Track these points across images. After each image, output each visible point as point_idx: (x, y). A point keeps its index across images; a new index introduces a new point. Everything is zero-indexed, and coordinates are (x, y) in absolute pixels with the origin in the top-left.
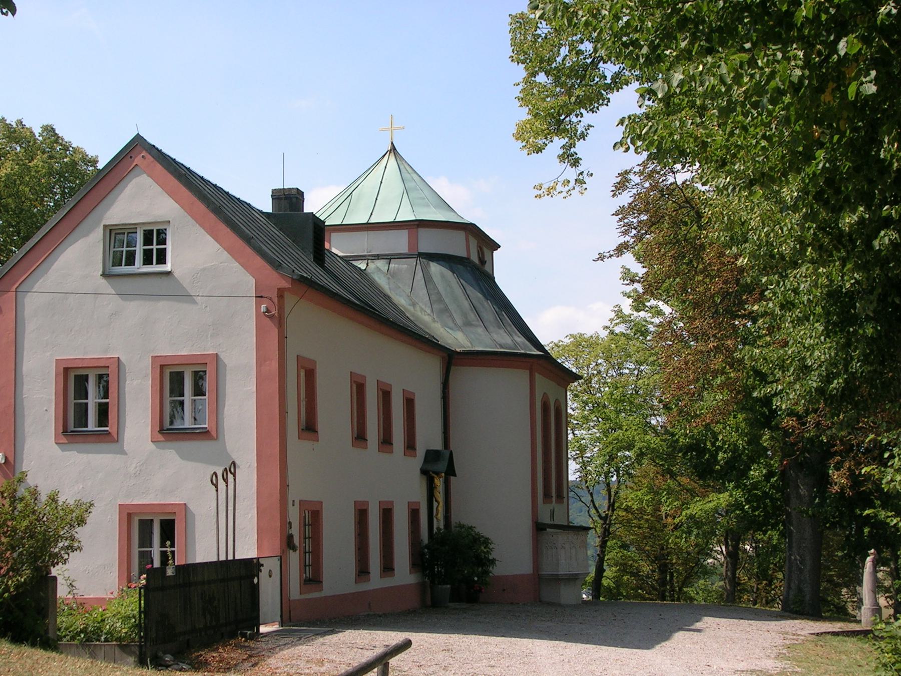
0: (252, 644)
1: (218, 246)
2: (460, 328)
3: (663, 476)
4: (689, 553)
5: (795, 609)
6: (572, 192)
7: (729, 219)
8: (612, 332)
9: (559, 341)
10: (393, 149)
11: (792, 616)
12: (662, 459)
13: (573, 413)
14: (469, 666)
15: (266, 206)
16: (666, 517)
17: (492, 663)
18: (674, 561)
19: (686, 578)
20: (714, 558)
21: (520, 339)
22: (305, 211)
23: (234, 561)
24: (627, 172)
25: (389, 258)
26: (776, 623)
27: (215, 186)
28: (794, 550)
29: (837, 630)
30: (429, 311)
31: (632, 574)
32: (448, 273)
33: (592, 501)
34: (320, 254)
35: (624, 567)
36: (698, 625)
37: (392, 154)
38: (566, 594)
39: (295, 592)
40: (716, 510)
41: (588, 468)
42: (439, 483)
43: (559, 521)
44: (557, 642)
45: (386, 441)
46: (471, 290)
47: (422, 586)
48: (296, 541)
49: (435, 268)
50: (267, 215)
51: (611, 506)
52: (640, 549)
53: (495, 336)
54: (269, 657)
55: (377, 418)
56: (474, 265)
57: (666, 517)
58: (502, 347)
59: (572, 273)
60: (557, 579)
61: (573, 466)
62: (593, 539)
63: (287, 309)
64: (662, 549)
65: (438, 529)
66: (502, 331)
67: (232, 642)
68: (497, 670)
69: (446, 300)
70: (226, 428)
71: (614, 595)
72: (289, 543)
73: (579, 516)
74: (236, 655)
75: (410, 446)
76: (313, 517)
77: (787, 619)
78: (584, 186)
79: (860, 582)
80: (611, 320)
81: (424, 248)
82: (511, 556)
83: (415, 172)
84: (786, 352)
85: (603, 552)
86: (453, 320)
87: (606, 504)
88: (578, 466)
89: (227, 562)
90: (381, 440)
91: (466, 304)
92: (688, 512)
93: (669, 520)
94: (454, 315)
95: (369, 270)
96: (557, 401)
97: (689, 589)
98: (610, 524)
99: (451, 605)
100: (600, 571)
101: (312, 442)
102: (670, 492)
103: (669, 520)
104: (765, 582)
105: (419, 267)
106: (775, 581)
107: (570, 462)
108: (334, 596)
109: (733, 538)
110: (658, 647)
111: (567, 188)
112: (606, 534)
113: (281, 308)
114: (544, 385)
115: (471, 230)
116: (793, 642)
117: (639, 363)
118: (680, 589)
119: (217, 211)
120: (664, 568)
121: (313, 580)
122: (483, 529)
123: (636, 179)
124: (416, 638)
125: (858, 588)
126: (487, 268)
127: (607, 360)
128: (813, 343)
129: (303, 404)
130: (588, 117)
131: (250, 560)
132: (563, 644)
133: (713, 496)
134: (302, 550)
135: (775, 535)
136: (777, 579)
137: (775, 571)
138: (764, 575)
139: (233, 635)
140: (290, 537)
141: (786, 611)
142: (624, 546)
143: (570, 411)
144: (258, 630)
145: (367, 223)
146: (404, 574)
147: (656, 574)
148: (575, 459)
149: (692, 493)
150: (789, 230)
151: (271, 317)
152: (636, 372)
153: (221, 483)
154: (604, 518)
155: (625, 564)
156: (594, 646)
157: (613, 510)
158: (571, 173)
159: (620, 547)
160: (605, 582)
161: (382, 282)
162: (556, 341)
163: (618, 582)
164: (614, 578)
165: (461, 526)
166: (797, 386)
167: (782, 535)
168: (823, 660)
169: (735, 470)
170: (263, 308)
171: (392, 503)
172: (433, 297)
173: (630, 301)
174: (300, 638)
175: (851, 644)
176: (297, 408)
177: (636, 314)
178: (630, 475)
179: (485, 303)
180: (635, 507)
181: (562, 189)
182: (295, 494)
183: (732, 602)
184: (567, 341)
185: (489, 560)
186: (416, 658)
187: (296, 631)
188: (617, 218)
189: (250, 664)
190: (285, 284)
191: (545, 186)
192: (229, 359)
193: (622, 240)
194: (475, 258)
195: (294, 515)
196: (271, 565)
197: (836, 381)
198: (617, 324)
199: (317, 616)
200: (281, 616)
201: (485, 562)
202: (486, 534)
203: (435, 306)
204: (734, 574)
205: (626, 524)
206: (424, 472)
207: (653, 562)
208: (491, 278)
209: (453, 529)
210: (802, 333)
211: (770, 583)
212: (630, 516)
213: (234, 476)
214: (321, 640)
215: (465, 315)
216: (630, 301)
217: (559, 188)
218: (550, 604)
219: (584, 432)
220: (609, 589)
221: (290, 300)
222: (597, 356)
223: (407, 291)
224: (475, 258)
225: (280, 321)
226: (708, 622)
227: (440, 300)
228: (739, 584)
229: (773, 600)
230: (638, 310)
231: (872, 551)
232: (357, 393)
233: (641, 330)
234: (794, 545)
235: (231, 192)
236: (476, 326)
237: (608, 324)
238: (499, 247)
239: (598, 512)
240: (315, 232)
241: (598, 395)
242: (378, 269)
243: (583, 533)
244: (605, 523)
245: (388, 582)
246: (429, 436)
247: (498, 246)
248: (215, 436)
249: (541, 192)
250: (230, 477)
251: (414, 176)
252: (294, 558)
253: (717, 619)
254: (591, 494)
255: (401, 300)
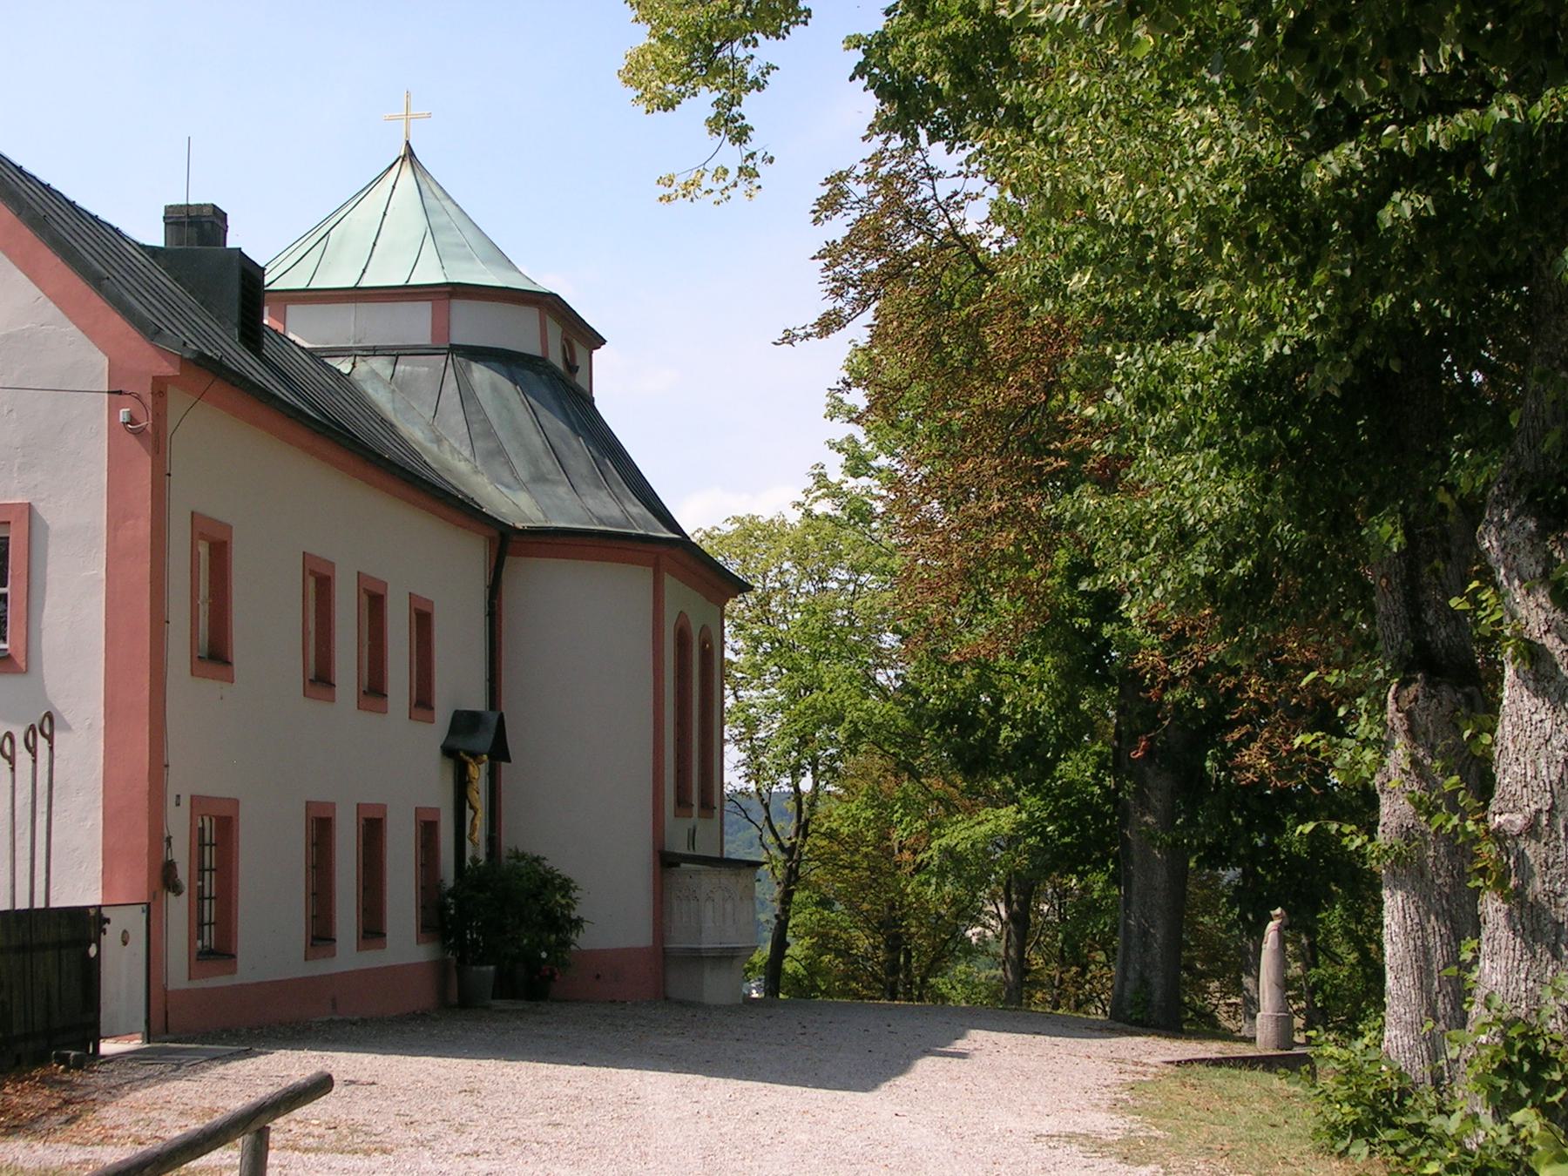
0: (76, 1077)
1: (37, 291)
2: (524, 486)
3: (896, 776)
4: (940, 917)
5: (1134, 1016)
6: (732, 192)
7: (1055, 187)
8: (808, 513)
9: (714, 529)
10: (410, 155)
11: (1129, 1028)
12: (895, 744)
13: (735, 659)
14: (510, 1124)
15: (153, 234)
16: (900, 851)
17: (557, 1118)
18: (913, 930)
19: (935, 960)
20: (984, 925)
21: (637, 509)
22: (229, 245)
23: (48, 911)
24: (841, 177)
25: (396, 353)
26: (1102, 1041)
27: (47, 187)
28: (1134, 908)
29: (1215, 1056)
30: (467, 453)
31: (838, 953)
32: (506, 385)
33: (768, 818)
34: (252, 335)
35: (824, 941)
36: (960, 1045)
37: (407, 162)
38: (715, 986)
39: (178, 973)
40: (991, 838)
41: (762, 759)
42: (478, 773)
43: (701, 850)
44: (689, 1076)
45: (374, 690)
46: (547, 417)
47: (441, 968)
48: (183, 873)
49: (481, 374)
50: (153, 251)
51: (803, 829)
52: (852, 906)
53: (590, 503)
54: (105, 1104)
55: (355, 646)
56: (550, 369)
57: (900, 851)
58: (601, 522)
59: (741, 408)
60: (696, 958)
61: (733, 755)
62: (768, 889)
63: (171, 423)
64: (892, 908)
65: (475, 860)
66: (603, 494)
67: (38, 1073)
68: (564, 1133)
69: (500, 434)
70: (44, 648)
71: (804, 989)
72: (167, 878)
73: (738, 845)
74: (38, 1099)
75: (423, 702)
76: (219, 831)
77: (1120, 1035)
78: (757, 181)
79: (1253, 967)
80: (807, 492)
81: (462, 335)
82: (613, 910)
83: (449, 198)
84: (1146, 505)
85: (785, 911)
86: (513, 471)
87: (791, 828)
88: (743, 756)
89: (31, 913)
90: (365, 687)
91: (537, 441)
92: (943, 841)
93: (907, 855)
94: (514, 461)
95: (356, 376)
96: (704, 628)
97: (940, 980)
98: (799, 862)
99: (499, 1004)
100: (780, 945)
101: (217, 684)
102: (906, 802)
103: (907, 855)
104: (1074, 969)
105: (450, 370)
106: (1092, 967)
107: (727, 748)
108: (259, 984)
109: (1022, 890)
110: (885, 1087)
111: (722, 185)
112: (792, 878)
113: (159, 416)
114: (681, 597)
115: (551, 306)
116: (1138, 1077)
117: (856, 569)
118: (924, 980)
119: (69, 255)
120: (895, 943)
121: (216, 950)
122: (561, 862)
123: (860, 190)
124: (340, 1063)
125: (1247, 981)
126: (580, 379)
127: (798, 562)
128: (1201, 488)
129: (204, 609)
130: (767, 49)
131: (83, 910)
132: (699, 1079)
133: (986, 813)
134: (195, 891)
135: (1098, 880)
136: (1095, 962)
137: (1092, 949)
138: (1073, 956)
139: (41, 1059)
140: (169, 868)
141: (1119, 1021)
142: (825, 903)
143: (728, 654)
144: (97, 1048)
145: (355, 288)
146: (405, 944)
147: (880, 953)
148: (737, 742)
149: (949, 807)
150: (1189, 196)
151: (137, 433)
152: (851, 587)
153: (23, 756)
154: (790, 851)
155: (827, 934)
156: (761, 1084)
157: (806, 835)
158: (732, 156)
159: (817, 904)
160: (789, 966)
161: (381, 397)
162: (708, 529)
163: (813, 968)
164: (806, 958)
165: (519, 856)
166: (1168, 574)
167: (1114, 880)
168: (1203, 1115)
169: (1032, 760)
170: (123, 415)
171: (383, 807)
172: (476, 428)
173: (842, 457)
174: (179, 1067)
175: (1249, 1082)
176: (190, 612)
177: (852, 482)
178: (834, 770)
179: (575, 444)
180: (845, 830)
181: (714, 186)
182: (180, 783)
183: (1017, 1002)
184: (729, 528)
185: (571, 921)
186: (404, 1108)
187: (175, 1051)
188: (821, 263)
189: (63, 1118)
190: (167, 369)
191: (680, 181)
192: (53, 514)
193: (828, 305)
194: (556, 359)
195: (179, 824)
196: (127, 921)
197: (1239, 564)
198: (817, 499)
199: (199, 1026)
200: (148, 1022)
201: (562, 924)
202: (565, 871)
203: (478, 444)
204: (1021, 952)
205: (829, 860)
206: (448, 751)
207: (876, 931)
208: (590, 401)
209: (504, 860)
210: (1180, 467)
211: (1084, 969)
212: (836, 848)
213: (51, 741)
214: (220, 1069)
215: (534, 461)
216: (842, 457)
217: (707, 183)
218: (681, 1003)
219: (755, 693)
220: (796, 979)
221: (177, 402)
222: (781, 555)
223: (422, 411)
224: (556, 359)
225: (157, 441)
226: (978, 1039)
227: (490, 433)
228: (1027, 972)
229: (1089, 1000)
230: (856, 475)
231: (1278, 911)
232: (371, 637)
233: (860, 513)
234: (1135, 898)
235: (79, 203)
236: (554, 482)
237: (802, 498)
238: (604, 342)
239: (777, 838)
240: (243, 287)
241: (783, 627)
242: (375, 374)
243: (746, 871)
244: (790, 859)
245: (373, 959)
246: (460, 682)
247: (601, 341)
248: (23, 665)
249: (671, 191)
250: (42, 743)
251: (447, 204)
252: (178, 908)
253: (994, 1035)
254: (766, 807)
255: (415, 432)
